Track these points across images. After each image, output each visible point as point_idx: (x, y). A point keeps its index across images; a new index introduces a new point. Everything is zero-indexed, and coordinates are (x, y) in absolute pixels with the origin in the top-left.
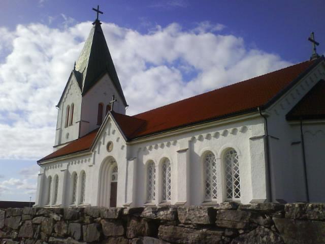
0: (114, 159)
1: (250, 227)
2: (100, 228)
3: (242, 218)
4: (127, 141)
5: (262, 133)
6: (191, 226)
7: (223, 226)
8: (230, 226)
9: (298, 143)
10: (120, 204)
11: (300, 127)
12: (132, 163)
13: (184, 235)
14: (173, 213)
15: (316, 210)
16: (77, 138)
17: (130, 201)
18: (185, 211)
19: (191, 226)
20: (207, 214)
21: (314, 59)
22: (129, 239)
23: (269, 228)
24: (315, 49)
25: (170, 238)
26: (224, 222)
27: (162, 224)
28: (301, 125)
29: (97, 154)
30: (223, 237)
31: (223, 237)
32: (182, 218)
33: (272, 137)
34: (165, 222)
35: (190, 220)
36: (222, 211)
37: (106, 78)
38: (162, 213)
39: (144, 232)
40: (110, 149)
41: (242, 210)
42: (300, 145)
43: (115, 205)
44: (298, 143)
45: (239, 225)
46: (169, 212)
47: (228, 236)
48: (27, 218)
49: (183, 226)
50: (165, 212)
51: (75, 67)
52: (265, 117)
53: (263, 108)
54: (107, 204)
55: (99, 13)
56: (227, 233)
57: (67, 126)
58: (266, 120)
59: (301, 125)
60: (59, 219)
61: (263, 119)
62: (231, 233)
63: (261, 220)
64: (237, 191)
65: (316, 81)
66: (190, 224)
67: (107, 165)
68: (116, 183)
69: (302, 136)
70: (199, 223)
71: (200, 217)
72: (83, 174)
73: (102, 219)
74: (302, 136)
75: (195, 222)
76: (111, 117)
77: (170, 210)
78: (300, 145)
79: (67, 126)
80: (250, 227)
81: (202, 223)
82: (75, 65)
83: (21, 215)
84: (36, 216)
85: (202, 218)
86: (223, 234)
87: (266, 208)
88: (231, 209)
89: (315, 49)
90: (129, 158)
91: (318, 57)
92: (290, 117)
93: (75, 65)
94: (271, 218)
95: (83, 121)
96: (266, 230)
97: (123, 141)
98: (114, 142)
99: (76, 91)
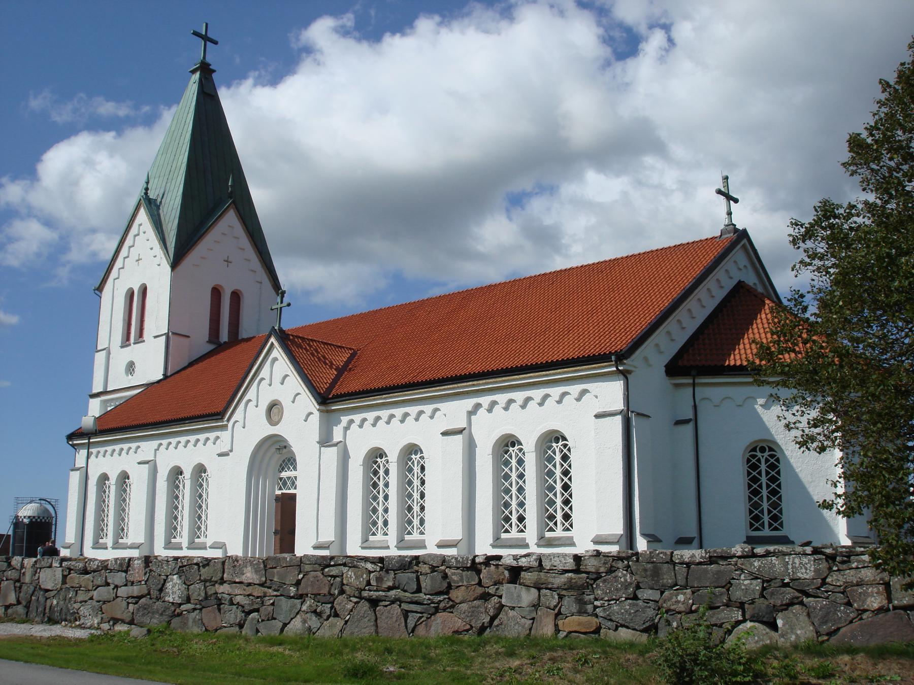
0: (285, 441)
1: (611, 570)
2: (445, 576)
3: (605, 563)
4: (320, 404)
5: (620, 405)
6: (556, 571)
7: (587, 570)
8: (594, 571)
9: (686, 422)
10: (304, 546)
11: (691, 389)
12: (331, 454)
13: (551, 580)
14: (536, 560)
15: (661, 555)
16: (162, 377)
17: (328, 534)
18: (549, 558)
19: (556, 571)
20: (572, 561)
21: (726, 236)
22: (485, 587)
23: (627, 571)
24: (730, 214)
25: (534, 584)
26: (588, 567)
27: (525, 571)
28: (694, 385)
29: (238, 426)
30: (588, 580)
31: (588, 580)
32: (547, 565)
33: (638, 414)
34: (528, 569)
35: (555, 566)
36: (586, 557)
37: (230, 220)
38: (523, 560)
39: (503, 579)
40: (275, 418)
41: (604, 556)
42: (690, 426)
43: (291, 549)
44: (686, 422)
45: (602, 570)
46: (532, 560)
47: (592, 579)
48: (311, 569)
49: (547, 572)
50: (528, 559)
51: (147, 189)
52: (625, 374)
53: (621, 357)
54: (265, 548)
55: (208, 43)
56: (591, 576)
57: (126, 341)
58: (627, 378)
59: (694, 385)
60: (378, 570)
61: (622, 377)
62: (594, 576)
63: (620, 564)
64: (567, 517)
65: (729, 285)
66: (555, 570)
67: (267, 450)
68: (293, 497)
69: (695, 407)
70: (564, 568)
71: (565, 563)
72: (200, 470)
73: (447, 567)
74: (695, 407)
75: (560, 568)
76: (276, 344)
77: (534, 557)
78: (690, 426)
79: (126, 341)
80: (611, 570)
81: (567, 568)
82: (147, 183)
83: (300, 566)
84: (329, 566)
85: (568, 564)
86: (588, 578)
87: (624, 555)
88: (595, 556)
89: (730, 214)
90: (325, 441)
91: (736, 230)
92: (674, 369)
93: (147, 183)
94: (628, 562)
95: (174, 334)
96: (625, 572)
97: (308, 402)
98: (286, 402)
99: (153, 253)
